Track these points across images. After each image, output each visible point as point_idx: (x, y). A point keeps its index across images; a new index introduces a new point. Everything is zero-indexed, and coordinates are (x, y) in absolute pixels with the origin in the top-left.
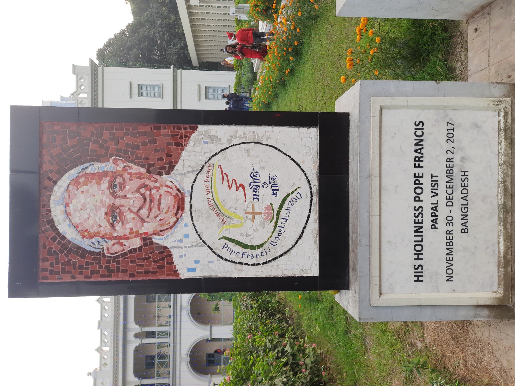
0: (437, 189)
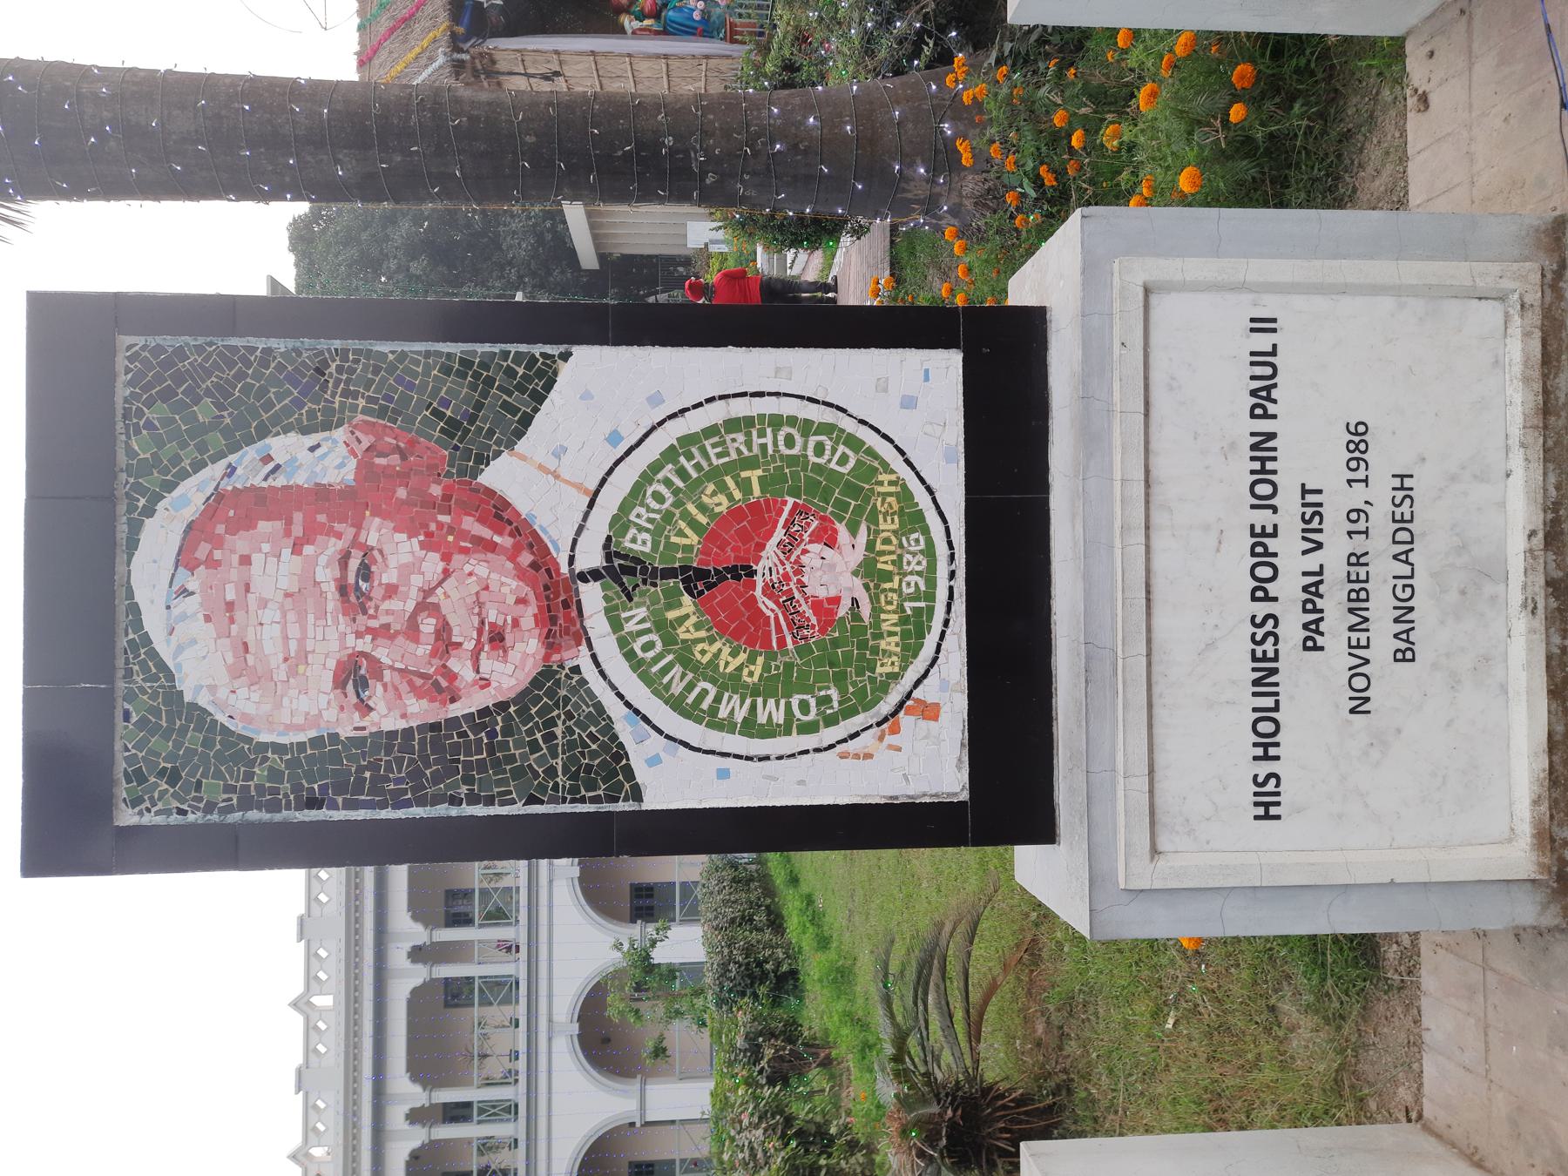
0: (1320, 531)
